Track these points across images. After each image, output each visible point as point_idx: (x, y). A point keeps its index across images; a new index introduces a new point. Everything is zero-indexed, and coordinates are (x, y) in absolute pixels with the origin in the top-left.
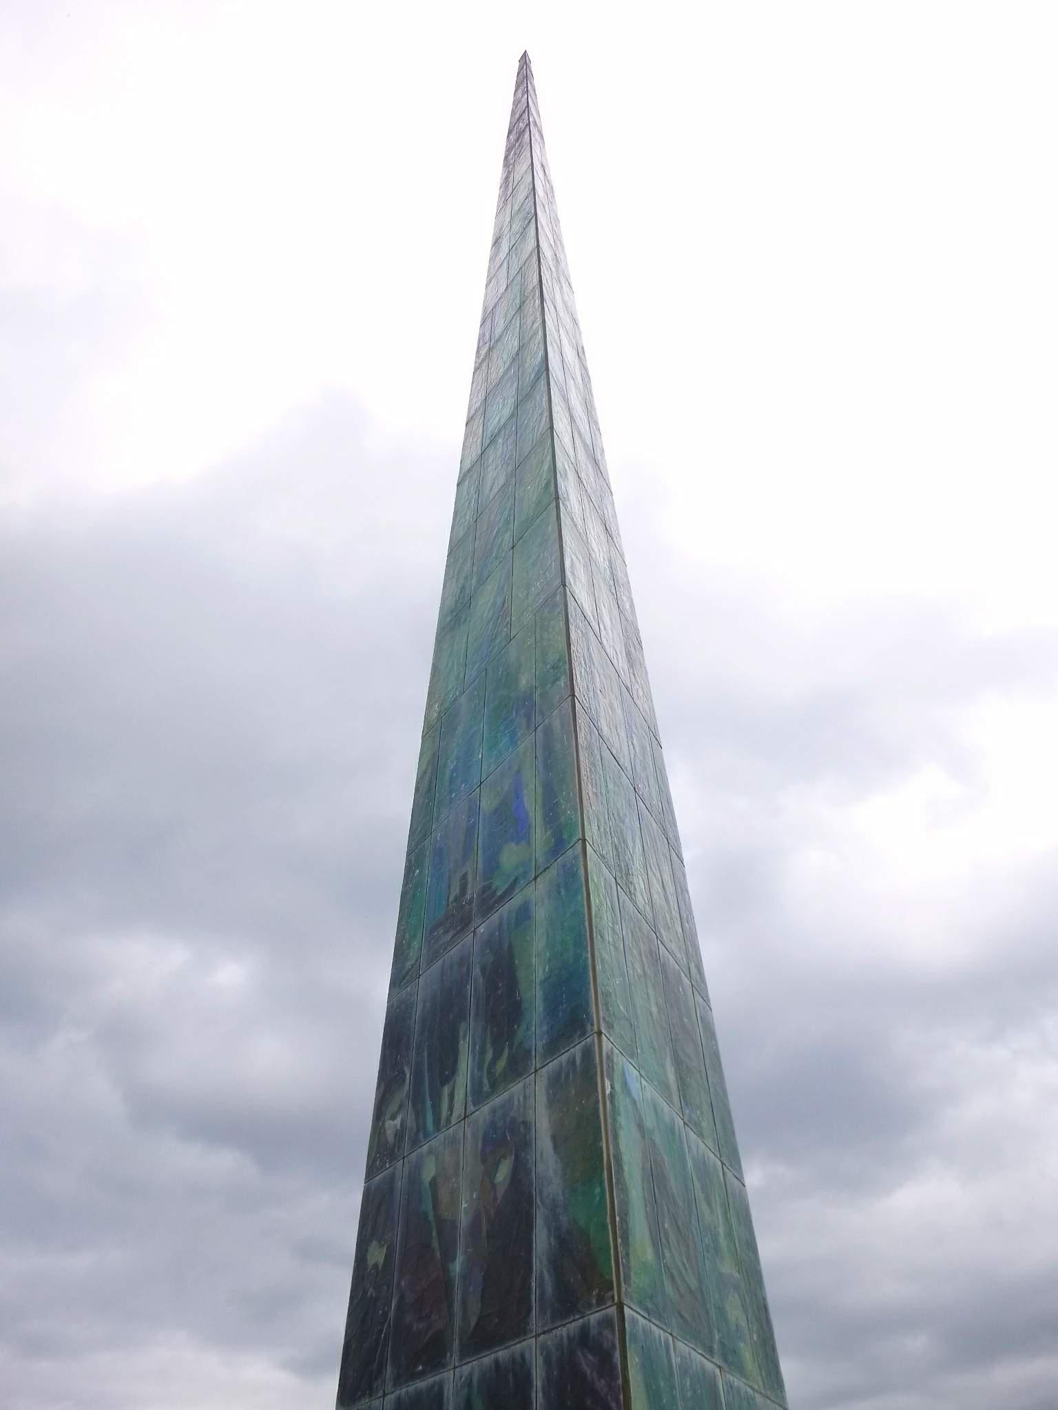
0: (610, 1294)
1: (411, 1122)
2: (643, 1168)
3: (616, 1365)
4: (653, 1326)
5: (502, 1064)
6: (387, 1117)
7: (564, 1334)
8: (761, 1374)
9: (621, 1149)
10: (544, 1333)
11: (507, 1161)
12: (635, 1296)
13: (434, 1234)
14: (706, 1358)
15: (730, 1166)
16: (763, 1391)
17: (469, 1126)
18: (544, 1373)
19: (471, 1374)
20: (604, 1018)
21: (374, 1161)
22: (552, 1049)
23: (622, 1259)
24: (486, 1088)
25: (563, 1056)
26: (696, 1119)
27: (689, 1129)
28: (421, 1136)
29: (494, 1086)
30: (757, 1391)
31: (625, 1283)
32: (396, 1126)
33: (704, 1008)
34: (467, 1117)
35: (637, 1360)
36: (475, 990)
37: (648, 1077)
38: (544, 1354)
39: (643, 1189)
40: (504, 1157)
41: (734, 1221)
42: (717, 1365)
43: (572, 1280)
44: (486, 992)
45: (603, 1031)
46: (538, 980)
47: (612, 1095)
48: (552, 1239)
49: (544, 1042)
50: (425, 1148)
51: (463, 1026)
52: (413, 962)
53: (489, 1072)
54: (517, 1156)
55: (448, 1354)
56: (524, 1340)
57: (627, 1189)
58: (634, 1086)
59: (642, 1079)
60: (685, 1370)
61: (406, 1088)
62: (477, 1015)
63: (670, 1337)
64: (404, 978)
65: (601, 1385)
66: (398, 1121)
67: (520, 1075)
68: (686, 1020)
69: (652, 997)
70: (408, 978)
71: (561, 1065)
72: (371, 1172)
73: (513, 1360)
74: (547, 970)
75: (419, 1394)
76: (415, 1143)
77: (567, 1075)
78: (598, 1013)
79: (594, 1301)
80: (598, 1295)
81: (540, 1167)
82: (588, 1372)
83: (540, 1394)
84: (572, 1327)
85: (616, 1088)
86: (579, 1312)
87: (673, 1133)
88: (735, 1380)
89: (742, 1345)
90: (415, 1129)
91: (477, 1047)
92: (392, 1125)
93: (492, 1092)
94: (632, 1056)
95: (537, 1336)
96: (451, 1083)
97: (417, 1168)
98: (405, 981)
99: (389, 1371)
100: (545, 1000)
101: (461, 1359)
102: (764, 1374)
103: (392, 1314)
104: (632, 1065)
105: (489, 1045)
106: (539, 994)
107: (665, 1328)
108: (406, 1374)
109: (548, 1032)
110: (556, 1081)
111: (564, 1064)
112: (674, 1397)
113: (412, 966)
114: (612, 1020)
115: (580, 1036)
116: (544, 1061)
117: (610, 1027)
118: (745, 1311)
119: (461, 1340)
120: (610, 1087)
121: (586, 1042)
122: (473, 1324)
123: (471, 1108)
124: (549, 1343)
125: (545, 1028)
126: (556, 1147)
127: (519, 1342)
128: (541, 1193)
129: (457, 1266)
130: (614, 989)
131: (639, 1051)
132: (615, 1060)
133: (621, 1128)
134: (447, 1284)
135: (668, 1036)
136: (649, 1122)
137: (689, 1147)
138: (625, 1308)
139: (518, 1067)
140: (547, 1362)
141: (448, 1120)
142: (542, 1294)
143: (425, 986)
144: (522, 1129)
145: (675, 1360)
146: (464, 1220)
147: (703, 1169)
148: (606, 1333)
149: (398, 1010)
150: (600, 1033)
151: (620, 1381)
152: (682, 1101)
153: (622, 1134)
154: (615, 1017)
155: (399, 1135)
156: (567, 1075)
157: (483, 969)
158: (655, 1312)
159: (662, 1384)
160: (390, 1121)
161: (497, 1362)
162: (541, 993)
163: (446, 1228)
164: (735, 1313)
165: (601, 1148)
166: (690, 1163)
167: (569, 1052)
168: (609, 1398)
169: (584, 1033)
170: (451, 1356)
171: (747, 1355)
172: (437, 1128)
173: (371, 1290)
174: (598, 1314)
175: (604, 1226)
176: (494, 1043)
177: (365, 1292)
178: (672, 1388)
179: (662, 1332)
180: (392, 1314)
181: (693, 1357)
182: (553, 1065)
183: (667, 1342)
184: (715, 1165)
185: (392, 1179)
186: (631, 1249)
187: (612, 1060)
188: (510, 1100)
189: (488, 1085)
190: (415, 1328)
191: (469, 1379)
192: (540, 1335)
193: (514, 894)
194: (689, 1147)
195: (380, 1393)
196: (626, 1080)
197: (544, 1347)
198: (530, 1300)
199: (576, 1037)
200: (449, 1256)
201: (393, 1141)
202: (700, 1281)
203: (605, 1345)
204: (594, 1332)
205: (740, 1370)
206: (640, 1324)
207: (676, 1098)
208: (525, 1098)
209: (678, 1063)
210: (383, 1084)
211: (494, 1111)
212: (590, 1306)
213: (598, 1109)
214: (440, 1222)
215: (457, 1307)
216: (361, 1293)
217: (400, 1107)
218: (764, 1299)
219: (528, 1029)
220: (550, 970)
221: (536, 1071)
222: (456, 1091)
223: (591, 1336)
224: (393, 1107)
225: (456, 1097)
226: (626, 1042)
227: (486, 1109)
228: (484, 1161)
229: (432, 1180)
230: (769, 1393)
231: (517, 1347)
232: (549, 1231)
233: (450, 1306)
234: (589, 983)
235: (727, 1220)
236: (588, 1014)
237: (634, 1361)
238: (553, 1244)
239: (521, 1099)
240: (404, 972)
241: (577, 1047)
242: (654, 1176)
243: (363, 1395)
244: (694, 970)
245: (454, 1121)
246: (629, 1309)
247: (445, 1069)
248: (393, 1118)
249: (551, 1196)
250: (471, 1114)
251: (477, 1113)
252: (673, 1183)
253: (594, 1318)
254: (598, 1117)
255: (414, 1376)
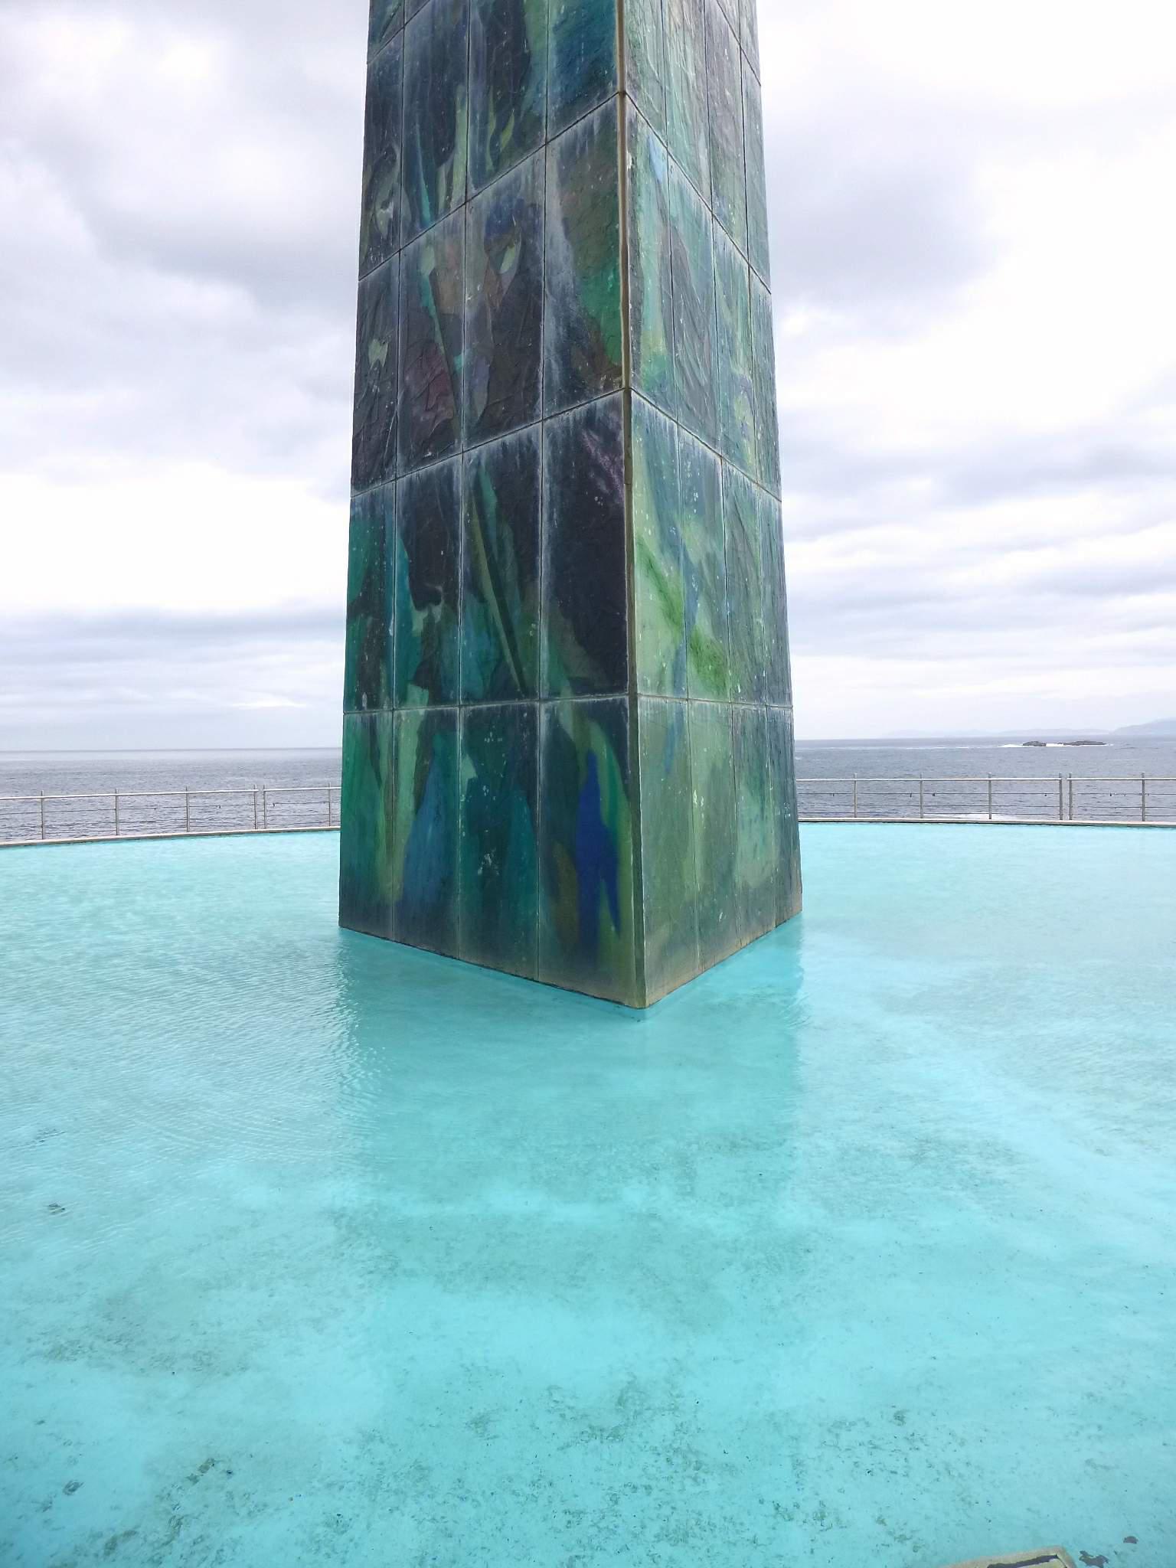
0: (618, 379)
1: (405, 211)
2: (662, 258)
3: (620, 443)
4: (659, 412)
5: (507, 136)
6: (378, 207)
7: (571, 418)
8: (761, 469)
9: (640, 233)
10: (551, 417)
11: (514, 250)
12: (643, 383)
13: (437, 329)
14: (709, 448)
15: (758, 270)
16: (759, 483)
17: (471, 212)
18: (550, 453)
19: (479, 458)
20: (629, 75)
21: (367, 257)
22: (567, 113)
23: (632, 346)
24: (490, 165)
25: (579, 124)
26: (726, 213)
27: (717, 223)
28: (417, 225)
29: (498, 162)
30: (754, 482)
31: (634, 369)
32: (388, 214)
33: (752, 81)
34: (470, 200)
35: (641, 439)
36: (474, 44)
37: (676, 157)
38: (550, 435)
39: (660, 280)
40: (510, 245)
41: (754, 328)
42: (719, 455)
43: (580, 368)
44: (487, 43)
45: (627, 91)
46: (551, 26)
47: (633, 172)
48: (561, 329)
49: (557, 106)
50: (422, 239)
51: (460, 89)
52: (396, 6)
53: (493, 146)
54: (524, 243)
55: (456, 441)
56: (531, 425)
57: (643, 278)
58: (660, 165)
59: (669, 157)
60: (686, 455)
61: (397, 170)
62: (477, 72)
63: (675, 424)
64: (385, 28)
65: (604, 460)
66: (390, 210)
67: (527, 149)
68: (728, 93)
69: (690, 60)
70: (390, 29)
71: (576, 135)
72: (364, 268)
73: (521, 444)
74: (562, 11)
75: (429, 477)
76: (411, 234)
77: (583, 149)
78: (624, 67)
79: (602, 387)
80: (607, 380)
81: (550, 255)
82: (593, 450)
83: (546, 470)
84: (579, 410)
85: (638, 164)
86: (586, 398)
87: (700, 226)
88: (734, 469)
89: (745, 441)
90: (410, 218)
91: (478, 117)
92: (384, 214)
93: (497, 171)
94: (660, 128)
95: (544, 420)
96: (450, 160)
97: (415, 262)
98: (386, 33)
99: (399, 459)
100: (560, 51)
101: (469, 444)
102: (763, 469)
103: (398, 408)
104: (659, 139)
105: (491, 114)
106: (552, 43)
107: (670, 415)
108: (416, 459)
109: (561, 94)
110: (570, 156)
111: (580, 133)
112: (674, 476)
113: (395, 11)
114: (639, 78)
115: (599, 99)
116: (556, 132)
117: (637, 87)
118: (753, 413)
119: (468, 428)
120: (631, 161)
121: (606, 106)
122: (480, 413)
123: (473, 191)
124: (556, 427)
125: (558, 89)
126: (567, 232)
127: (526, 427)
128: (550, 283)
129: (462, 360)
130: (644, 38)
131: (668, 123)
132: (639, 130)
133: (640, 209)
134: (454, 376)
135: (704, 108)
136: (674, 210)
137: (715, 243)
138: (633, 392)
139: (525, 140)
140: (553, 443)
141: (447, 207)
142: (550, 380)
143: (410, 42)
144: (530, 212)
145: (679, 446)
146: (468, 313)
147: (728, 268)
148: (612, 415)
149: (381, 73)
150: (623, 94)
151: (623, 457)
152: (713, 190)
153: (641, 216)
154: (643, 76)
155: (393, 225)
156: (583, 149)
157: (483, 12)
158: (661, 395)
159: (663, 462)
160: (382, 210)
161: (504, 444)
162: (555, 44)
163: (449, 323)
164: (742, 412)
165: (617, 231)
166: (714, 260)
167: (586, 118)
168: (612, 471)
169: (605, 93)
170: (459, 442)
171: (749, 451)
172: (435, 216)
173: (375, 387)
174: (605, 398)
175: (616, 314)
176: (498, 108)
177: (370, 388)
178: (673, 467)
179: (667, 419)
180: (398, 408)
181: (696, 445)
182: (566, 136)
183: (672, 428)
184: (741, 267)
185: (387, 275)
186: (642, 338)
187: (636, 132)
188: (517, 178)
189: (491, 164)
190: (422, 419)
191: (477, 462)
192: (546, 419)
193: (403, 189)
194: (715, 243)
195: (393, 478)
196: (650, 156)
197: (550, 430)
198: (537, 388)
199: (595, 99)
200: (453, 349)
201: (387, 233)
202: (711, 378)
203: (610, 427)
204: (599, 415)
205: (742, 463)
206: (646, 409)
207: (706, 187)
208: (534, 176)
209: (712, 143)
210: (369, 167)
211: (498, 193)
212: (597, 391)
213: (616, 186)
214: (442, 316)
215: (463, 395)
216: (365, 390)
217: (392, 193)
218: (774, 404)
219: (538, 90)
220: (566, 12)
221: (547, 143)
222: (455, 170)
223: (597, 418)
224: (383, 195)
225: (455, 179)
226: (654, 109)
227: (489, 191)
228: (488, 250)
229: (431, 275)
230: (765, 485)
231: (523, 432)
232: (558, 320)
233: (457, 397)
234: (614, 29)
235: (746, 326)
236: (610, 68)
237: (637, 440)
238: (562, 333)
239: (529, 177)
240: (384, 23)
241: (596, 112)
242: (674, 268)
243: (376, 480)
244: (745, 30)
245: (453, 206)
246: (635, 394)
247: (441, 145)
248: (385, 205)
249: (561, 285)
250: (473, 198)
251: (479, 196)
252: (694, 282)
253: (600, 402)
254: (616, 195)
255: (424, 461)
